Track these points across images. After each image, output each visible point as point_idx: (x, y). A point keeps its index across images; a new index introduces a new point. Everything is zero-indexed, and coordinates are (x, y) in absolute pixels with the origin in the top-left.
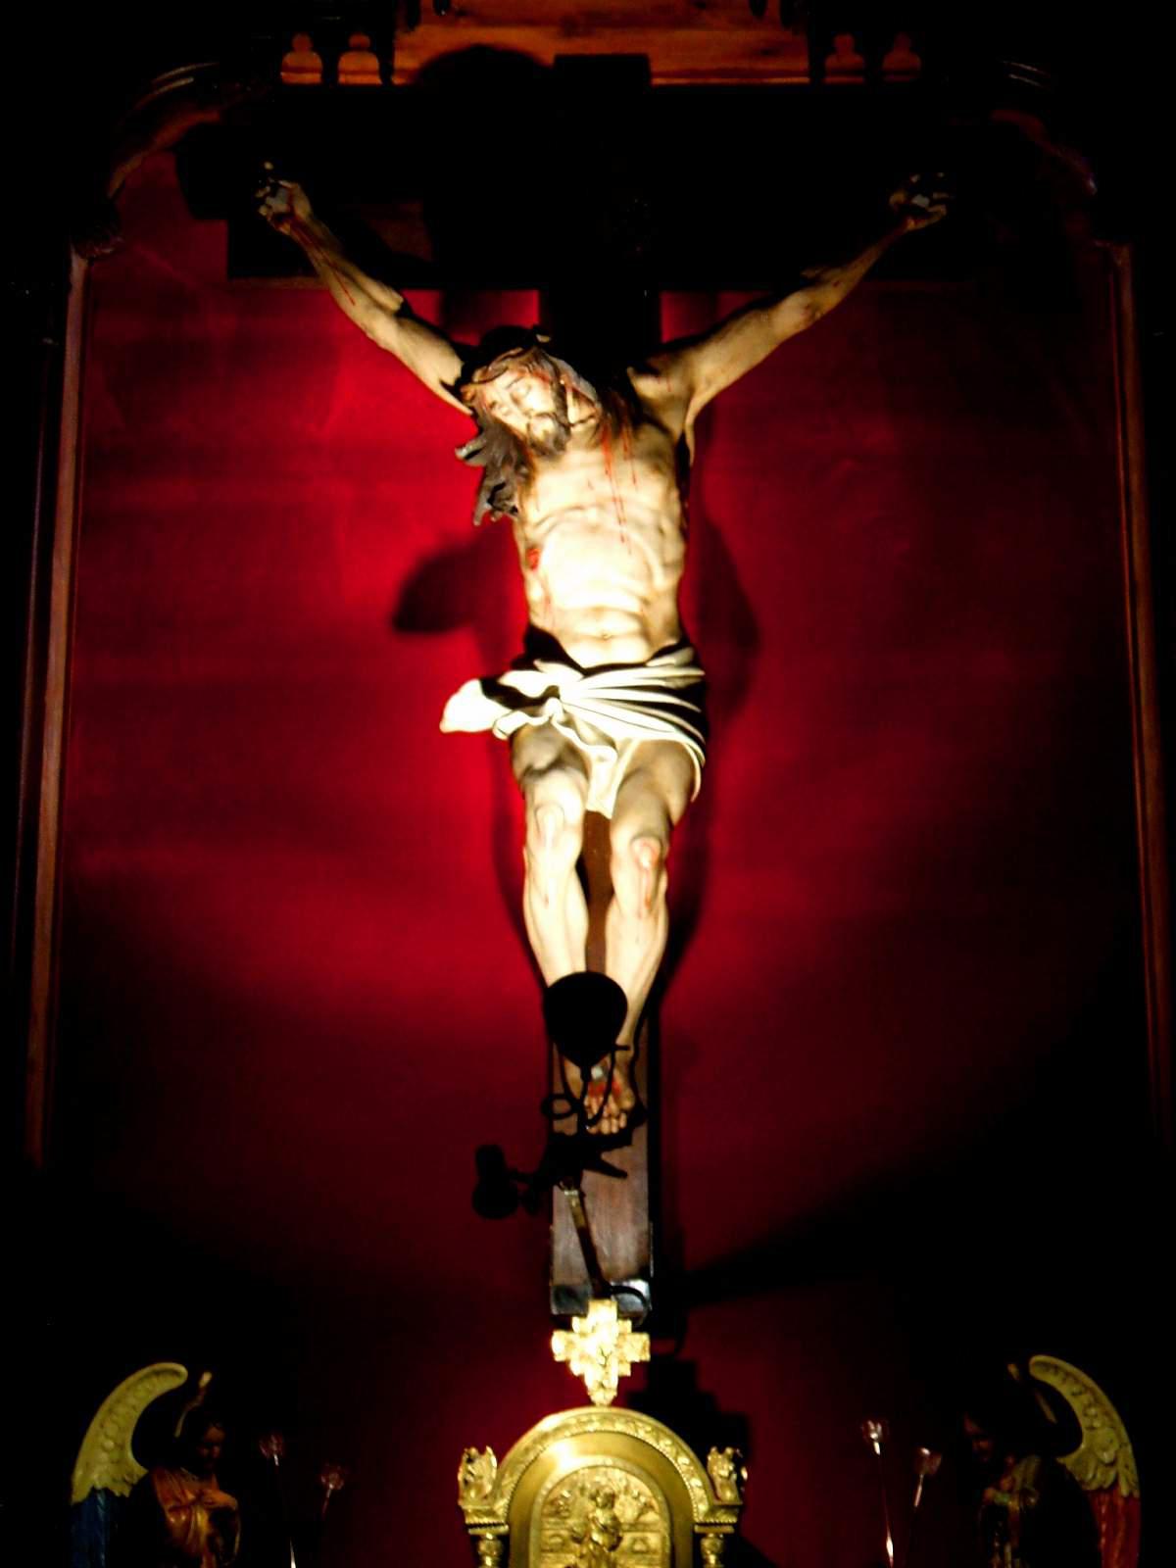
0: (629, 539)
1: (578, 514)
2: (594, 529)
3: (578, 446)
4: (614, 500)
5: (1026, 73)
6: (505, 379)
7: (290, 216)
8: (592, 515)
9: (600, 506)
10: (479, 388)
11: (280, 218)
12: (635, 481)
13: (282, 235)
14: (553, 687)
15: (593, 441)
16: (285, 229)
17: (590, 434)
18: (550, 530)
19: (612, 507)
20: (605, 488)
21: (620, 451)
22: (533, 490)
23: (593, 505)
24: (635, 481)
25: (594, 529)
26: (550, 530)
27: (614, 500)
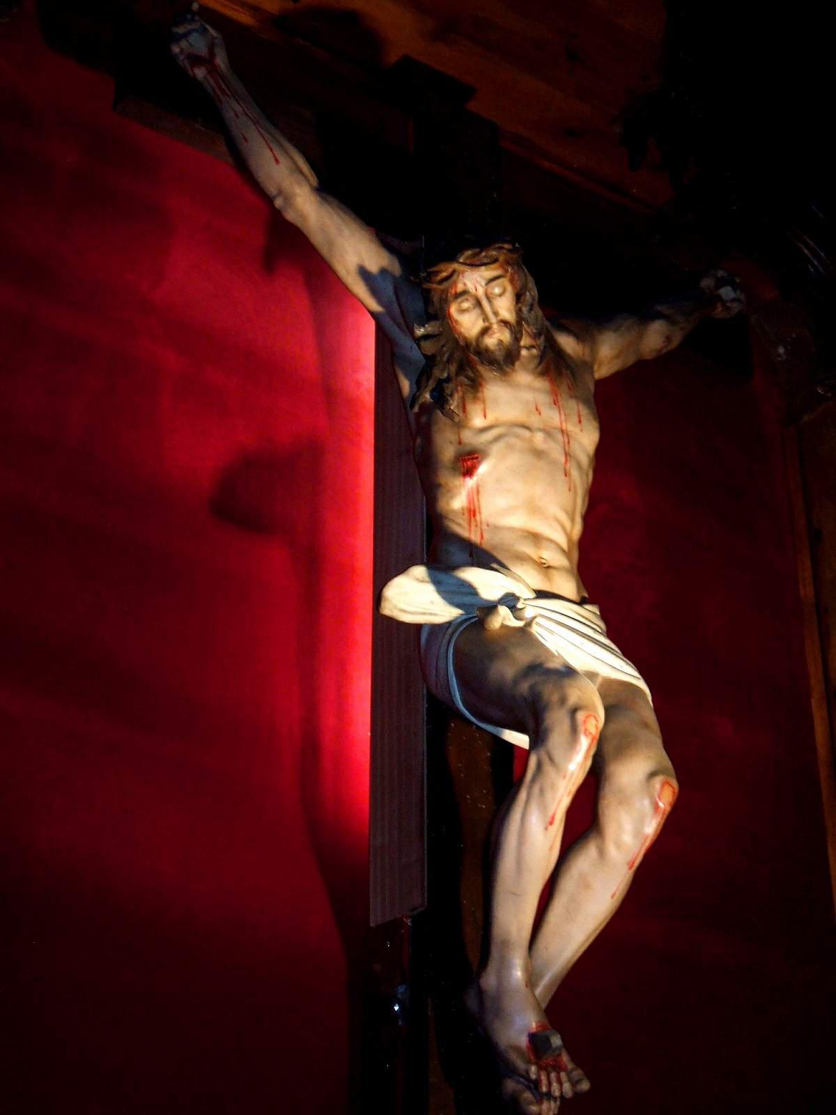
0: (570, 475)
1: (526, 433)
2: (538, 454)
3: (525, 368)
4: (562, 431)
5: (809, 248)
6: (487, 273)
7: (207, 61)
8: (539, 438)
9: (548, 433)
10: (462, 268)
11: (196, 60)
12: (580, 422)
13: (194, 78)
14: (513, 595)
15: (540, 369)
16: (200, 73)
17: (536, 361)
18: (498, 439)
19: (559, 436)
20: (553, 417)
21: (564, 388)
22: (480, 395)
23: (540, 430)
24: (580, 422)
25: (538, 454)
26: (498, 439)
27: (562, 431)
